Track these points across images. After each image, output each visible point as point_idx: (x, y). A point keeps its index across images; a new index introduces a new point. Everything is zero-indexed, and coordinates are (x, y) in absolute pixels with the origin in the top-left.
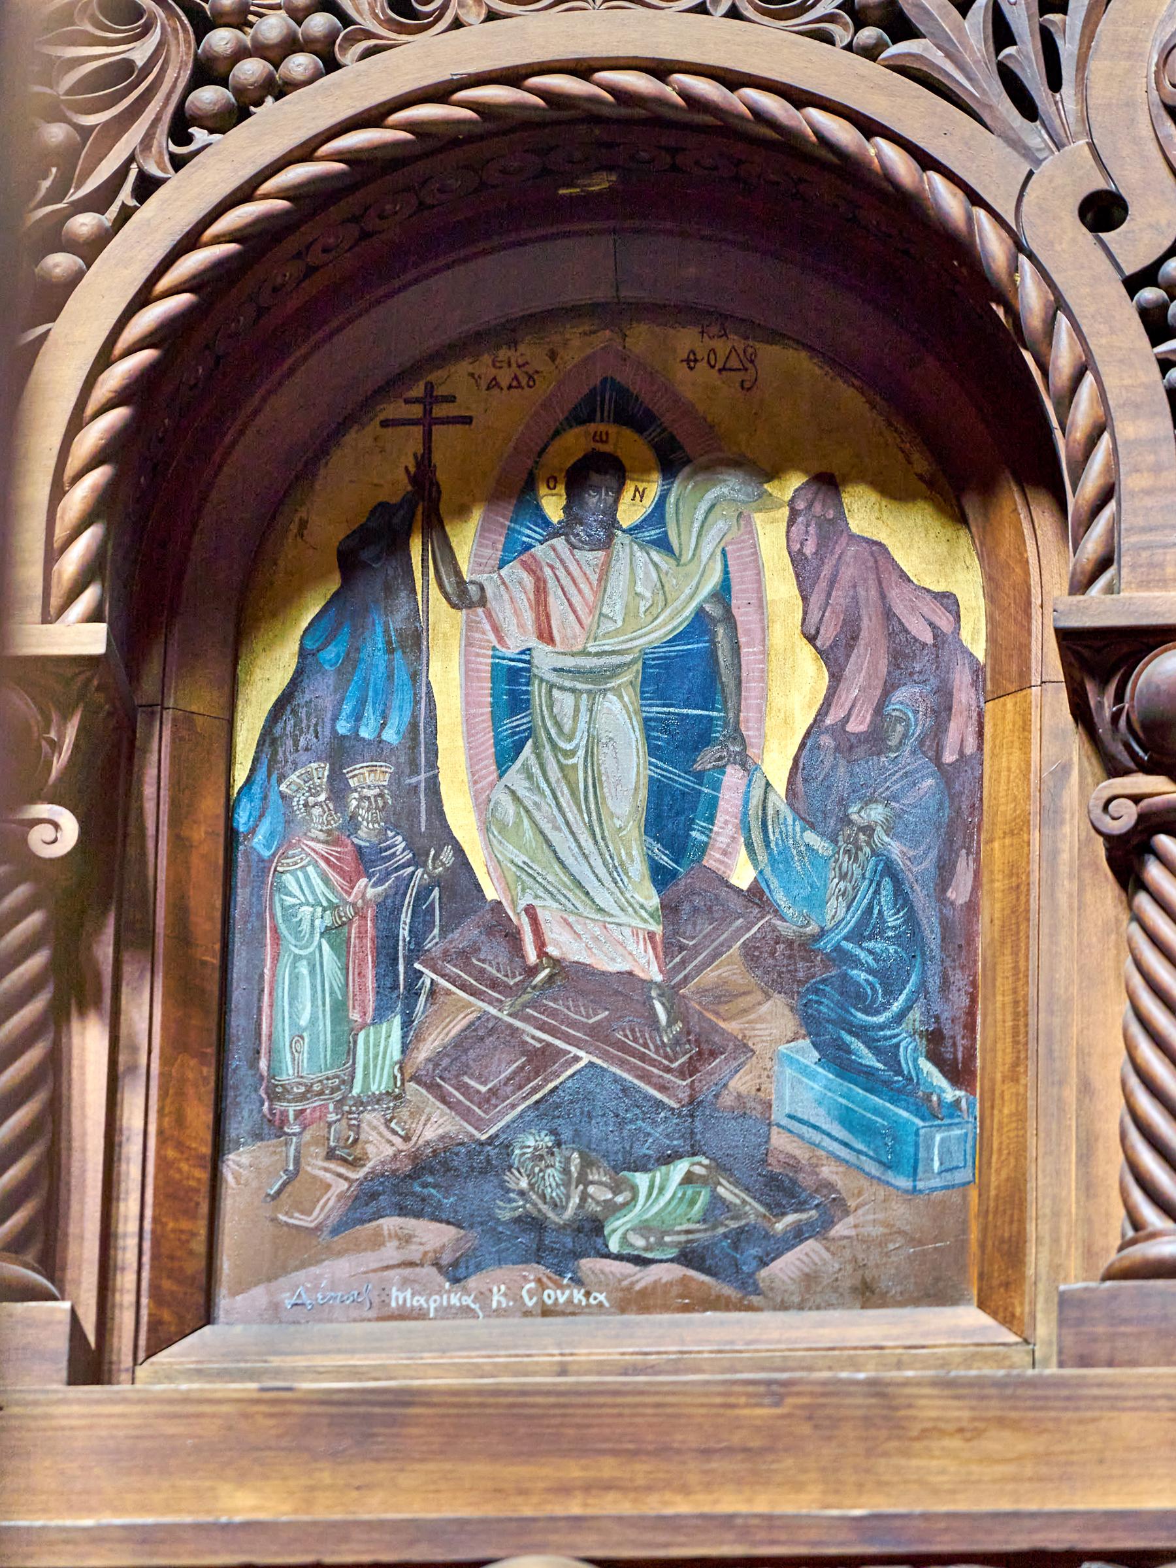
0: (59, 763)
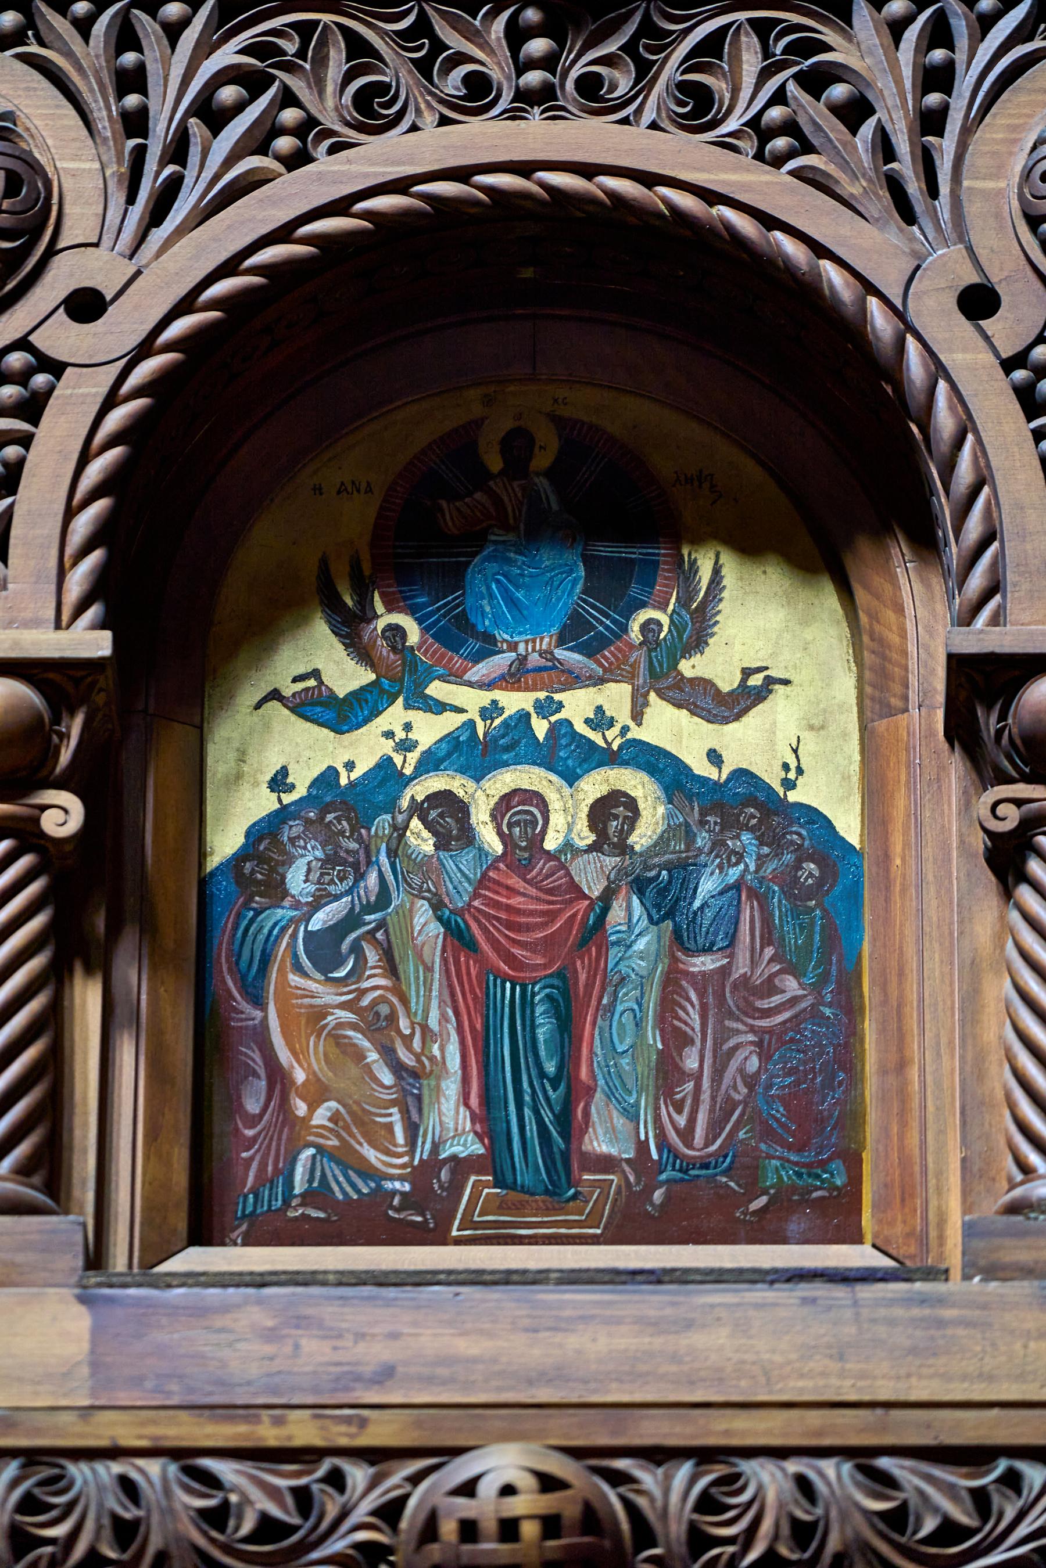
0: (65, 757)
